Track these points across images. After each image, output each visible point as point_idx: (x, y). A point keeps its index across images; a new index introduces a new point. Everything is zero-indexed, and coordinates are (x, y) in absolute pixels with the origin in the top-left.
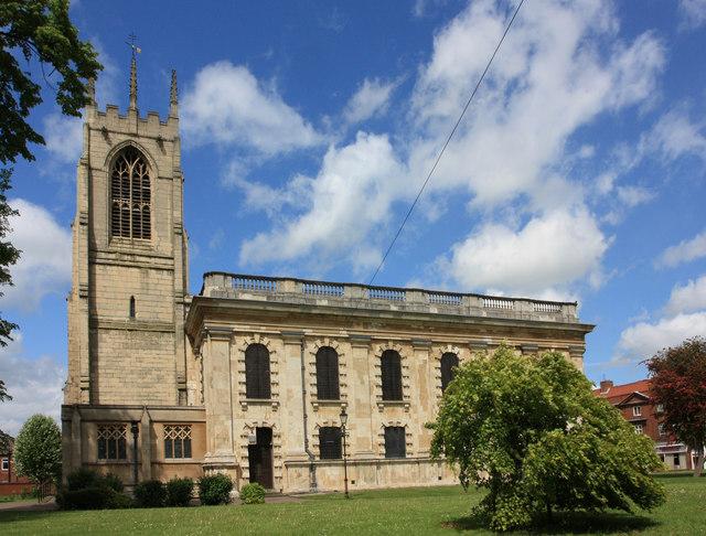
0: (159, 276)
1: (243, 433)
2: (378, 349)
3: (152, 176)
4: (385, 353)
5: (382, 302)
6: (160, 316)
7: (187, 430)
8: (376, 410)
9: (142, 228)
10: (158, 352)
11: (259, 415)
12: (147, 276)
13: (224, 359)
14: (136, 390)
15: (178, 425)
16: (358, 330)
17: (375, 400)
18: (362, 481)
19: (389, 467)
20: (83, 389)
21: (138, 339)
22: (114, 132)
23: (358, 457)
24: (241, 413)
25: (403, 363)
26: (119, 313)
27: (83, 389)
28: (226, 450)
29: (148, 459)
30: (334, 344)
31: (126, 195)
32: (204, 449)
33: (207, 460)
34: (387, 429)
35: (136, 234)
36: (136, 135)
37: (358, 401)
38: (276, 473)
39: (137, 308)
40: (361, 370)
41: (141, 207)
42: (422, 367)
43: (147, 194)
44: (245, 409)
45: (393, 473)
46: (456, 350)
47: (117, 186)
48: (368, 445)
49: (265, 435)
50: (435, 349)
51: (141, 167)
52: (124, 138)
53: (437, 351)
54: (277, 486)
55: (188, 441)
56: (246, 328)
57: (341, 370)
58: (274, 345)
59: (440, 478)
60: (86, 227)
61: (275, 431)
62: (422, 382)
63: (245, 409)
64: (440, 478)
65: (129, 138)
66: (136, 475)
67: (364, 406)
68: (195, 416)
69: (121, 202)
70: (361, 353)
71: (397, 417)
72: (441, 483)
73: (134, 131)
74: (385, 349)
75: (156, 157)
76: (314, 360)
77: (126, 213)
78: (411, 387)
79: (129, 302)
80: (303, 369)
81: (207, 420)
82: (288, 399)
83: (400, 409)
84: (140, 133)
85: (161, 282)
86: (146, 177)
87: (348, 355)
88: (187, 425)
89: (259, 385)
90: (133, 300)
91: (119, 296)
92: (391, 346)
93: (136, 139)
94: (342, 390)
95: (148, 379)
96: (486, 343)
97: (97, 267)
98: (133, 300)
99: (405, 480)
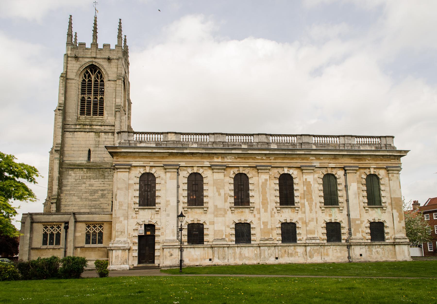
0: (106, 137)
1: (135, 227)
2: (232, 173)
3: (105, 80)
4: (237, 175)
5: (100, 119)
6: (106, 159)
7: (101, 227)
8: (229, 212)
9: (99, 109)
10: (103, 180)
11: (147, 216)
12: (99, 136)
13: (125, 185)
14: (87, 203)
15: (95, 224)
16: (217, 160)
17: (228, 205)
18: (269, 257)
19: (238, 250)
20: (52, 203)
21: (90, 174)
22: (83, 57)
23: (214, 243)
24: (134, 216)
25: (250, 181)
26: (81, 159)
27: (52, 203)
28: (122, 239)
29: (72, 245)
30: (201, 171)
31: (90, 92)
32: (110, 238)
33: (110, 245)
34: (236, 224)
35: (95, 114)
36: (95, 58)
37: (216, 206)
38: (157, 253)
39: (92, 155)
40: (218, 186)
41: (99, 98)
42: (264, 184)
43: (102, 93)
44: (137, 213)
45: (240, 254)
46: (291, 172)
47: (85, 87)
48: (223, 235)
49: (150, 227)
50: (276, 170)
51: (99, 76)
52: (87, 60)
53: (276, 173)
54: (157, 262)
55: (101, 234)
56: (141, 164)
57: (205, 187)
58: (158, 173)
59: (277, 258)
60: (61, 112)
61: (157, 227)
62: (264, 193)
63: (137, 213)
64: (210, 260)
65: (91, 60)
66: (360, 244)
67: (220, 209)
68: (106, 218)
69: (86, 97)
70: (219, 176)
71: (244, 216)
72: (277, 262)
73: (95, 56)
74: (237, 173)
75: (107, 70)
76: (186, 181)
77: (89, 102)
78: (210, 192)
79: (87, 152)
80: (178, 187)
81: (112, 220)
82: (167, 206)
83: (247, 210)
84: (98, 56)
85: (107, 140)
86: (102, 81)
87: (210, 178)
88: (101, 224)
89: (147, 196)
90: (89, 151)
91: (81, 149)
92: (241, 171)
93: (96, 60)
94: (205, 200)
95: (96, 196)
96: (315, 166)
97: (67, 133)
98: (89, 151)
99: (249, 258)
